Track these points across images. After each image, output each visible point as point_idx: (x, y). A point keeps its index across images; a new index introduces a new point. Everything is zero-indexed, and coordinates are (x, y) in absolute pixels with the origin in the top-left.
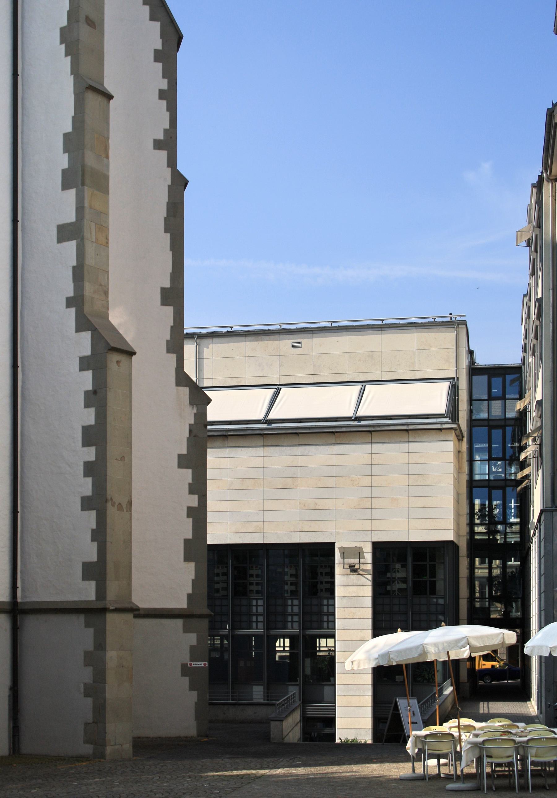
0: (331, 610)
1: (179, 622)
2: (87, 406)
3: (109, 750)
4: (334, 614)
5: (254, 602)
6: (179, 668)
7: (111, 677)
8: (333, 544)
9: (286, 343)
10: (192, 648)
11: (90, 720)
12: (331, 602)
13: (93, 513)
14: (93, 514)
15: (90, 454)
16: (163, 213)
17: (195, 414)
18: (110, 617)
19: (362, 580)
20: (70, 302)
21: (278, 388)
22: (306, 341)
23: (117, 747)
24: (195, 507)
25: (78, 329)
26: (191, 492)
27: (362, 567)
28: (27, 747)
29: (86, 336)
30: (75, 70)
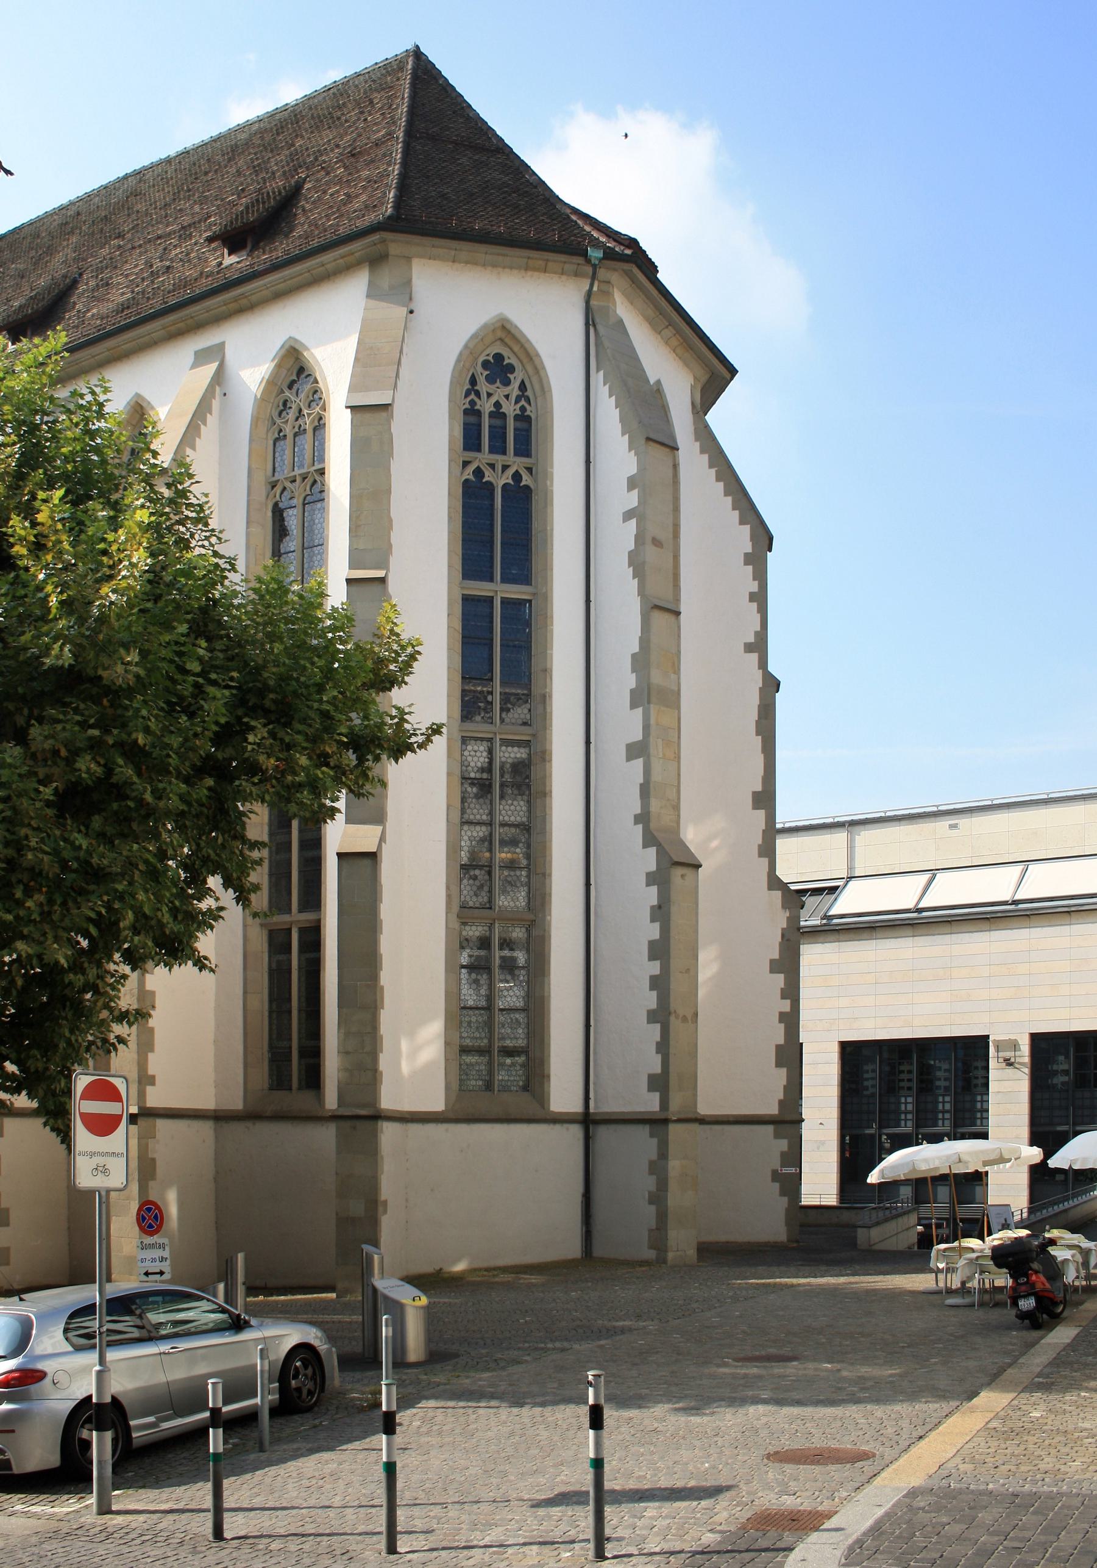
0: (984, 1107)
1: (770, 1129)
2: (653, 920)
3: (670, 1255)
4: (987, 1111)
5: (903, 1100)
6: (769, 1174)
7: (673, 1186)
8: (988, 1036)
9: (943, 824)
10: (783, 1154)
11: (654, 1227)
12: (985, 1098)
13: (658, 1026)
14: (657, 1027)
15: (655, 968)
16: (755, 716)
17: (788, 918)
18: (672, 1127)
19: (1017, 1074)
20: (638, 819)
21: (933, 872)
22: (963, 822)
23: (678, 1253)
24: (787, 1013)
25: (645, 846)
26: (783, 997)
27: (1018, 1060)
28: (598, 1251)
29: (652, 851)
30: (641, 592)
